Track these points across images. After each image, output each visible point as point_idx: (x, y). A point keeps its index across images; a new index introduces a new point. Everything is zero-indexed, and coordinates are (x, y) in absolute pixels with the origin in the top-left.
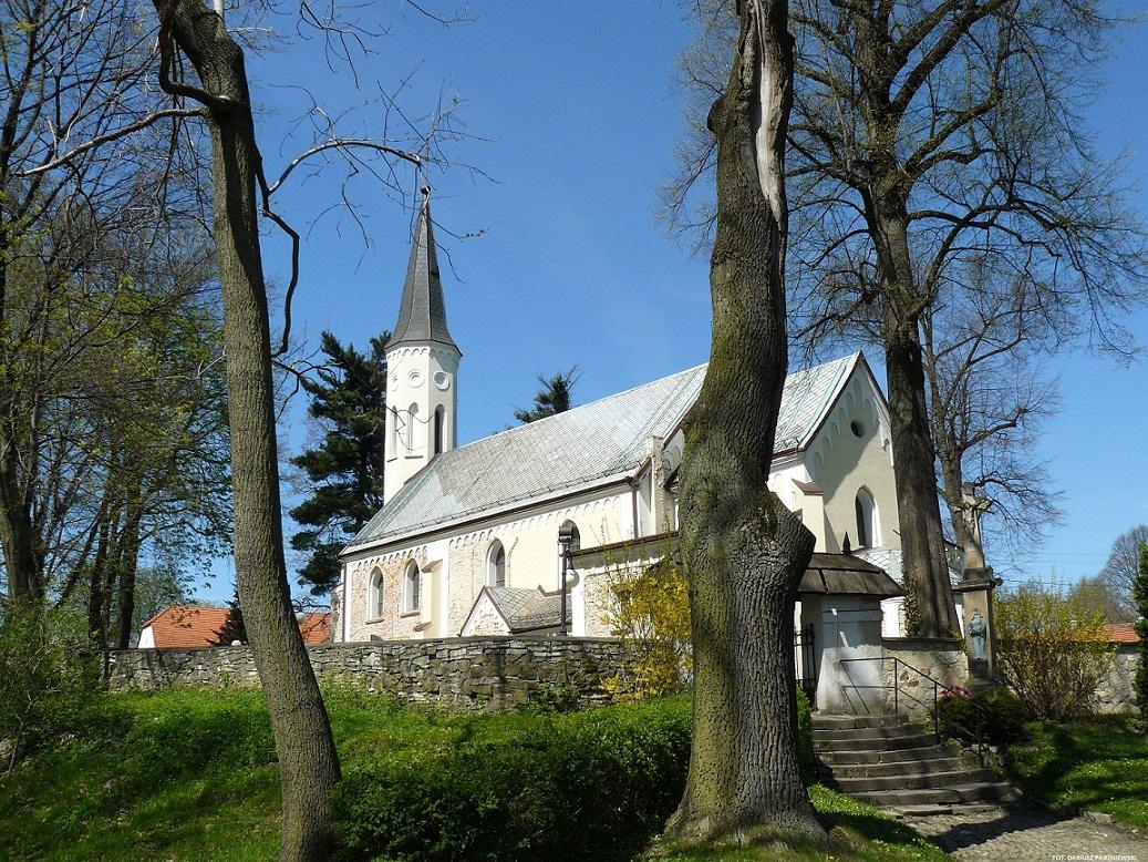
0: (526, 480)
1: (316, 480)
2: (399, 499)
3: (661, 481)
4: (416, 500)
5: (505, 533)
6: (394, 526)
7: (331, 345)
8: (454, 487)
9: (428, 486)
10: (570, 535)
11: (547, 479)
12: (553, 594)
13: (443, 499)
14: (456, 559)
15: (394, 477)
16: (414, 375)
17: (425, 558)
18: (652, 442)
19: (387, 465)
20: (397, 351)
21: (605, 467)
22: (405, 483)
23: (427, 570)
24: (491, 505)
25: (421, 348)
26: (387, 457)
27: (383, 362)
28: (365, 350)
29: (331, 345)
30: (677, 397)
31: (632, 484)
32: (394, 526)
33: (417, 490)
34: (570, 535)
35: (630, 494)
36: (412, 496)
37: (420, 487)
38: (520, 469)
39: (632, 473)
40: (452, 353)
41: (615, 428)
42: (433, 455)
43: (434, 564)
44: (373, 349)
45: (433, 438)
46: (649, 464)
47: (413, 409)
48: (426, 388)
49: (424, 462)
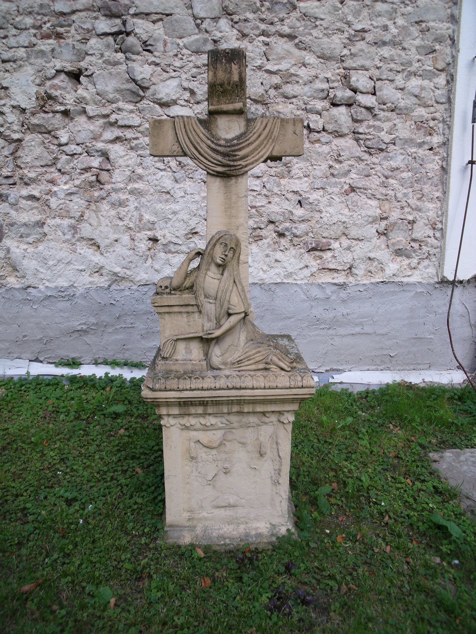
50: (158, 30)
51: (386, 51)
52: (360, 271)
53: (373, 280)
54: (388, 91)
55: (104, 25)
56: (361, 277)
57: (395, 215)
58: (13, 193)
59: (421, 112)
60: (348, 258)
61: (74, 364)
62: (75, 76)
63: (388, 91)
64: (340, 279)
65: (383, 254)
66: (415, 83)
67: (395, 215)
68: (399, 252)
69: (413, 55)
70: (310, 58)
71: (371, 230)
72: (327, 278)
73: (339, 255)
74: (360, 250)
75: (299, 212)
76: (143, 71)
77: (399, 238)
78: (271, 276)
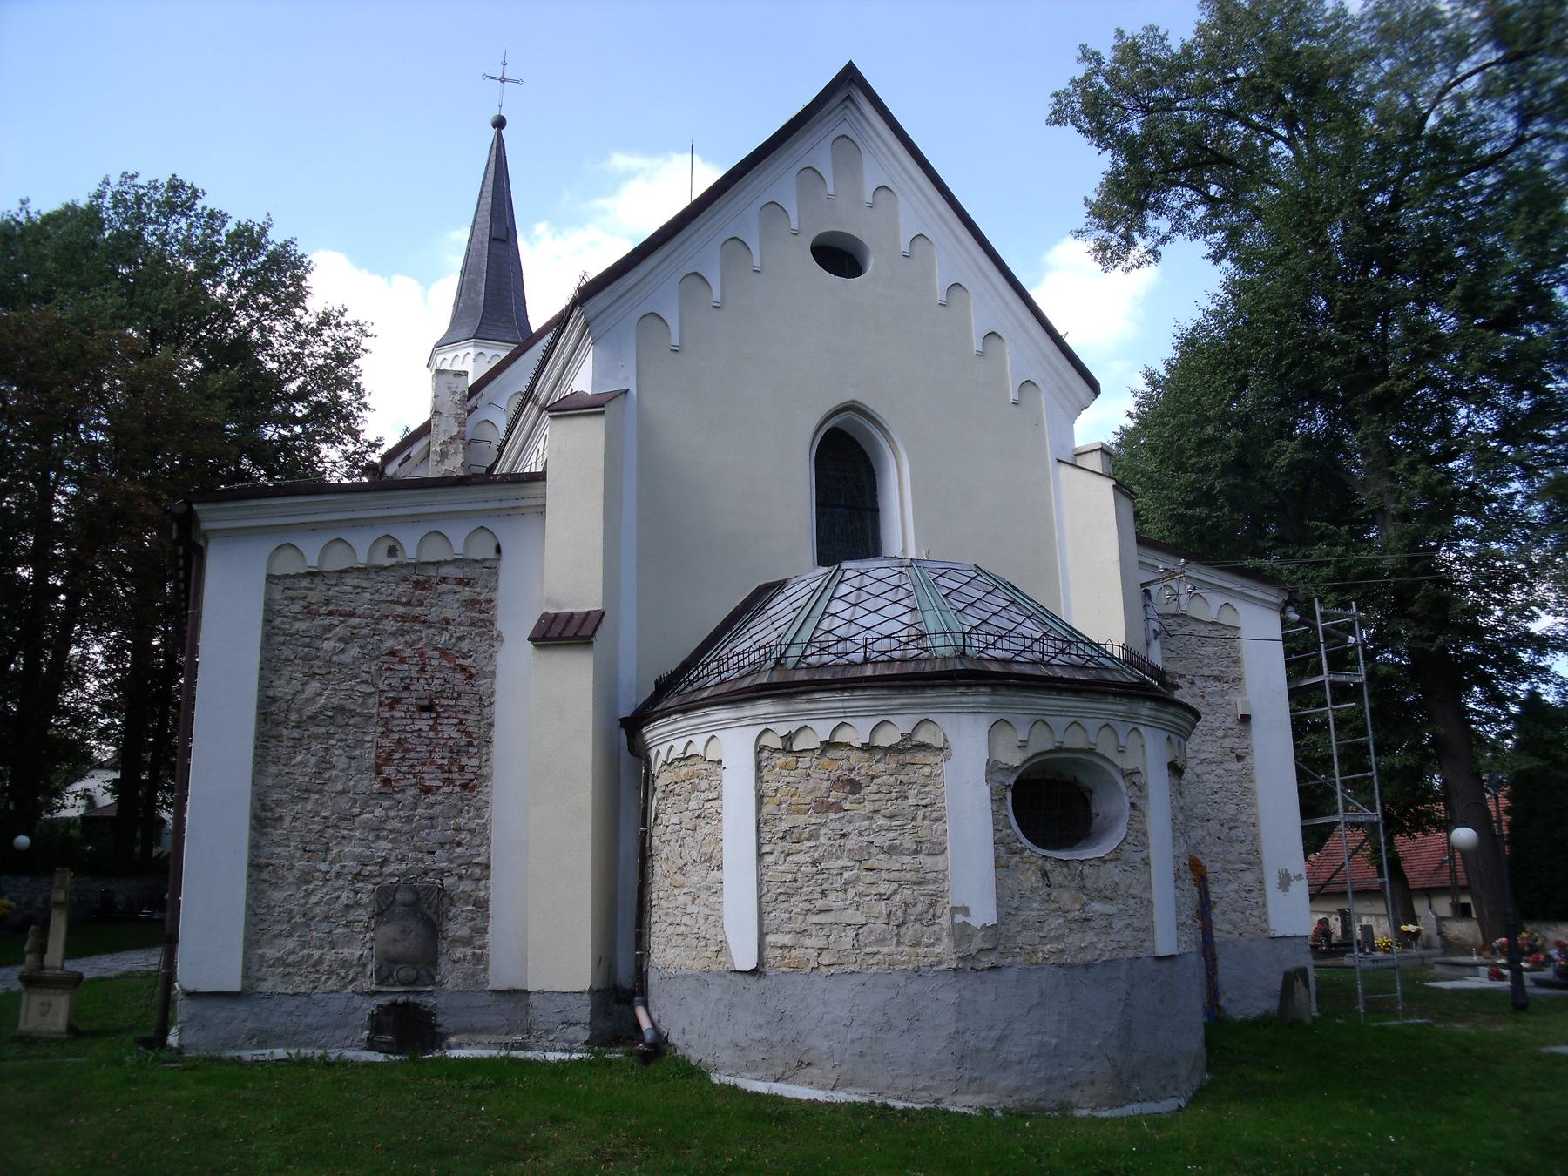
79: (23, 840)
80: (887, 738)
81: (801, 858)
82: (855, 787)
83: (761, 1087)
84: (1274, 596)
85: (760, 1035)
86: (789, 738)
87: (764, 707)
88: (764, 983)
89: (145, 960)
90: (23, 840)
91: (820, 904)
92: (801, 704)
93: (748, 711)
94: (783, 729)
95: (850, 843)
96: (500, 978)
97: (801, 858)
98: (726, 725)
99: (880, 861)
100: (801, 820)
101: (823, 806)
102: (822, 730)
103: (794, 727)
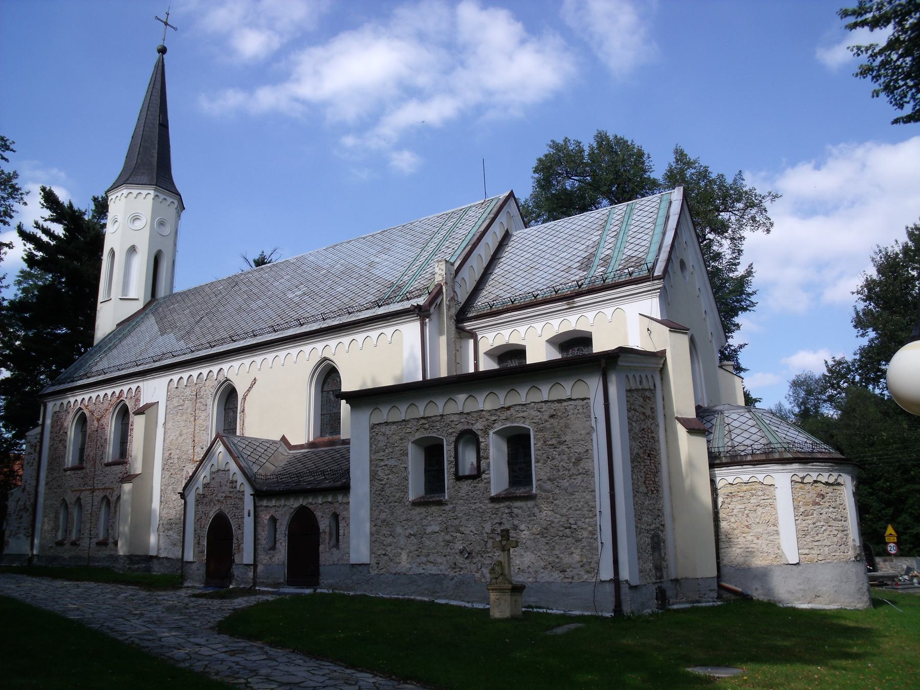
0: (263, 316)
1: (489, 609)
2: (110, 340)
3: (453, 311)
4: (129, 340)
5: (236, 371)
6: (100, 366)
7: (50, 199)
8: (173, 326)
9: (143, 327)
10: (328, 374)
11: (292, 314)
12: (301, 447)
13: (161, 339)
14: (175, 402)
15: (107, 318)
16: (136, 218)
17: (138, 400)
18: (443, 267)
19: (99, 306)
20: (119, 194)
21: (372, 298)
22: (118, 325)
23: (140, 412)
24: (223, 341)
25: (144, 192)
26: (101, 298)
27: (103, 222)
28: (85, 206)
29: (50, 199)
30: (451, 231)
31: (421, 313)
32: (103, 364)
33: (130, 332)
34: (328, 374)
35: (417, 325)
36: (125, 337)
37: (134, 328)
38: (254, 306)
39: (421, 301)
40: (176, 202)
41: (372, 264)
42: (149, 298)
43: (148, 406)
44: (93, 208)
45: (155, 375)
46: (440, 292)
47: (133, 250)
48: (146, 234)
49: (139, 305)
50: (520, 511)
51: (578, 512)
52: (576, 578)
53: (327, 541)
54: (580, 523)
55: (507, 511)
56: (576, 580)
57: (585, 560)
58: (484, 555)
59: (590, 528)
60: (571, 574)
61: (699, 602)
62: (500, 524)
63: (580, 523)
64: (570, 580)
65: (582, 573)
66: (587, 520)
67: (585, 560)
68: (588, 572)
69: (586, 512)
70: (558, 516)
71: (578, 565)
72: (566, 580)
73: (569, 573)
74: (575, 571)
75: (557, 560)
76: (516, 522)
77: (587, 567)
78: (550, 580)
79: (18, 343)
80: (831, 480)
81: (809, 522)
82: (823, 496)
83: (419, 598)
84: (850, 468)
85: (801, 587)
86: (803, 478)
87: (795, 466)
88: (800, 568)
89: (892, 548)
90: (18, 343)
91: (817, 538)
92: (809, 466)
93: (788, 467)
94: (801, 475)
95: (823, 516)
96: (673, 577)
97: (809, 522)
98: (776, 471)
99: (832, 523)
100: (808, 508)
101: (815, 503)
102: (814, 476)
103: (805, 474)
